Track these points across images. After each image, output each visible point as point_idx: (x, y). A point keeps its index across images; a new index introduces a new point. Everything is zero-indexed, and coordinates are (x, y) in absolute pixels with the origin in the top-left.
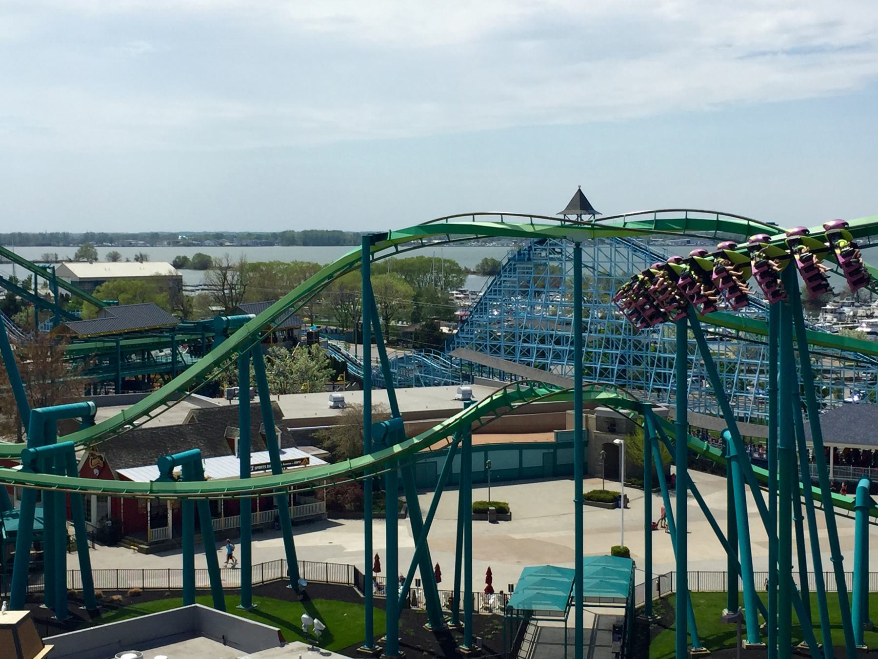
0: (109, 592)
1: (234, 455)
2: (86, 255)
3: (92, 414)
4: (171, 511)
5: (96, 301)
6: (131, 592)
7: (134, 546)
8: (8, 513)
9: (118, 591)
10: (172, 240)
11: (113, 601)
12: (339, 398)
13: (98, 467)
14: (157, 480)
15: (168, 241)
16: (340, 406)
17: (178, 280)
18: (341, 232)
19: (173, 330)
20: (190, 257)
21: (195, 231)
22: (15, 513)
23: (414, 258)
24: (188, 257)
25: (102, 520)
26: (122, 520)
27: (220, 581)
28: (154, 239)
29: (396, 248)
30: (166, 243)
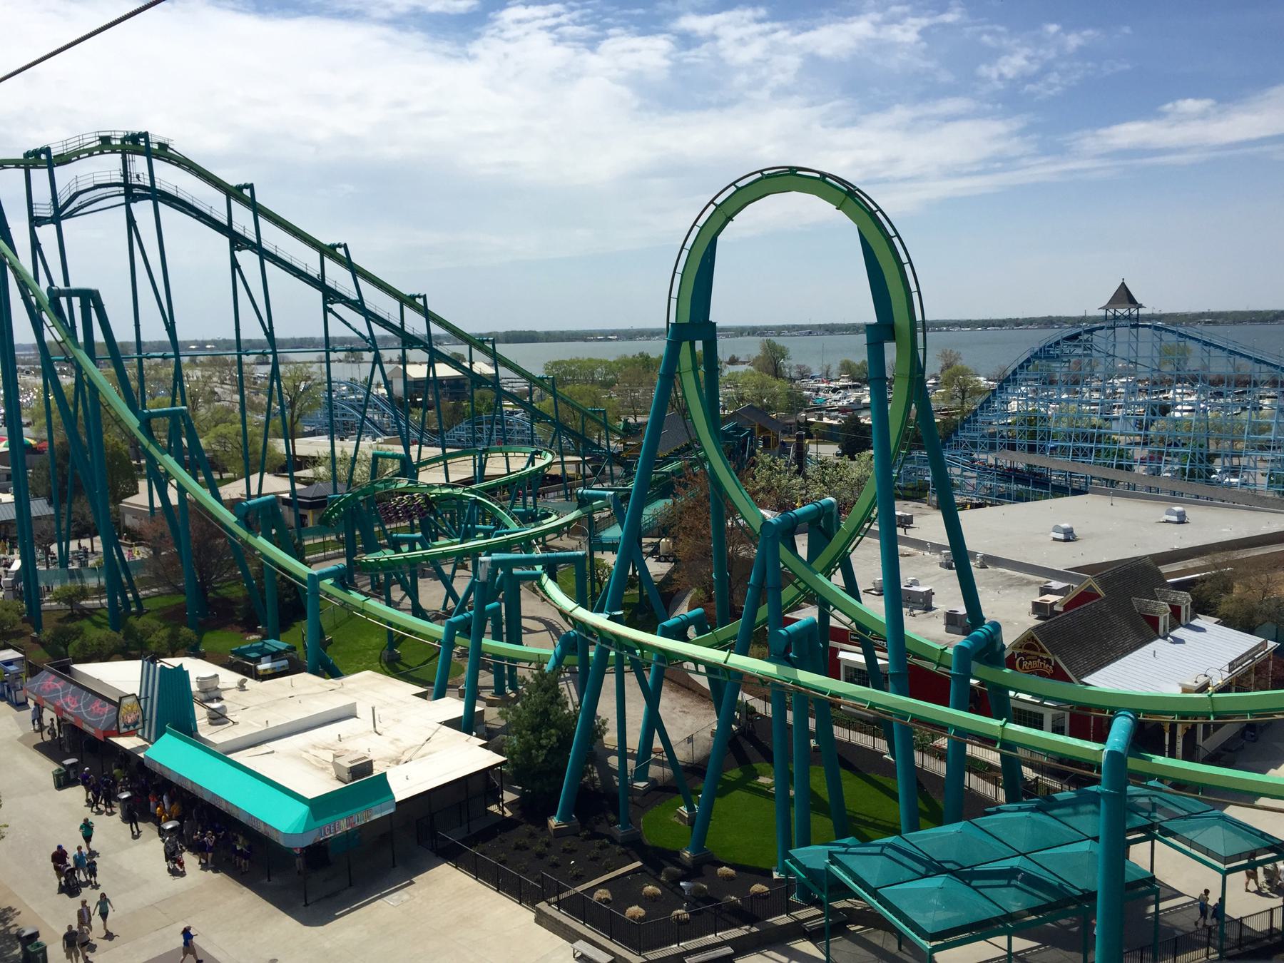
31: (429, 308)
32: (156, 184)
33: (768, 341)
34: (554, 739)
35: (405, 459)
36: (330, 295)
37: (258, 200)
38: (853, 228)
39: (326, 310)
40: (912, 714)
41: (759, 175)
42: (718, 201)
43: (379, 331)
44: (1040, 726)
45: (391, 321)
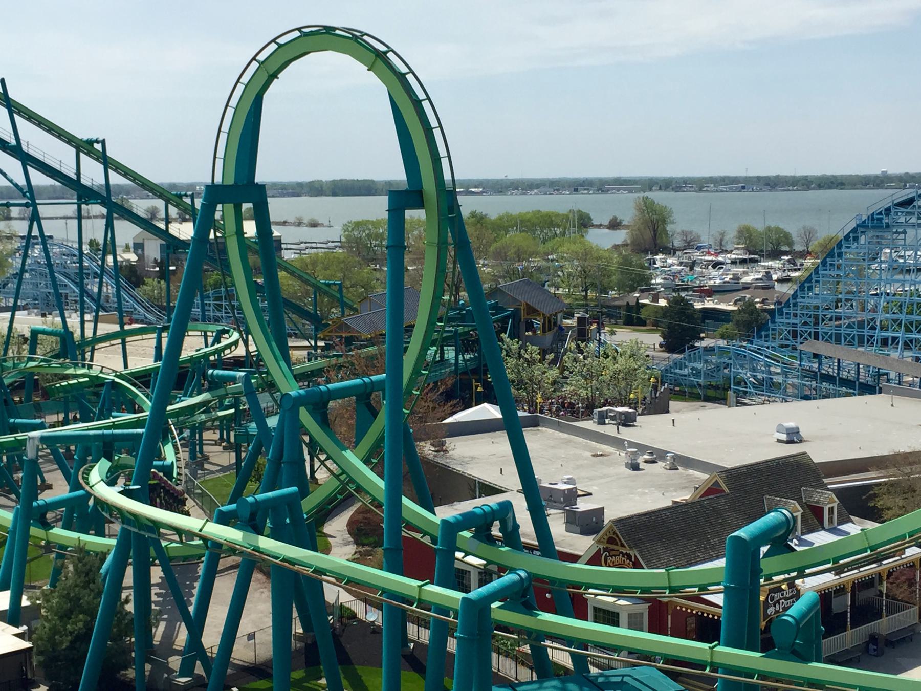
12: (793, 429)
16: (795, 440)
18: (373, 181)
21: (674, 176)
23: (529, 213)
27: (407, 634)
29: (258, 62)
33: (645, 199)
34: (80, 625)
35: (65, 336)
38: (384, 89)
40: (349, 577)
41: (297, 34)
42: (261, 57)
43: (39, 179)
44: (616, 623)
45: (64, 171)
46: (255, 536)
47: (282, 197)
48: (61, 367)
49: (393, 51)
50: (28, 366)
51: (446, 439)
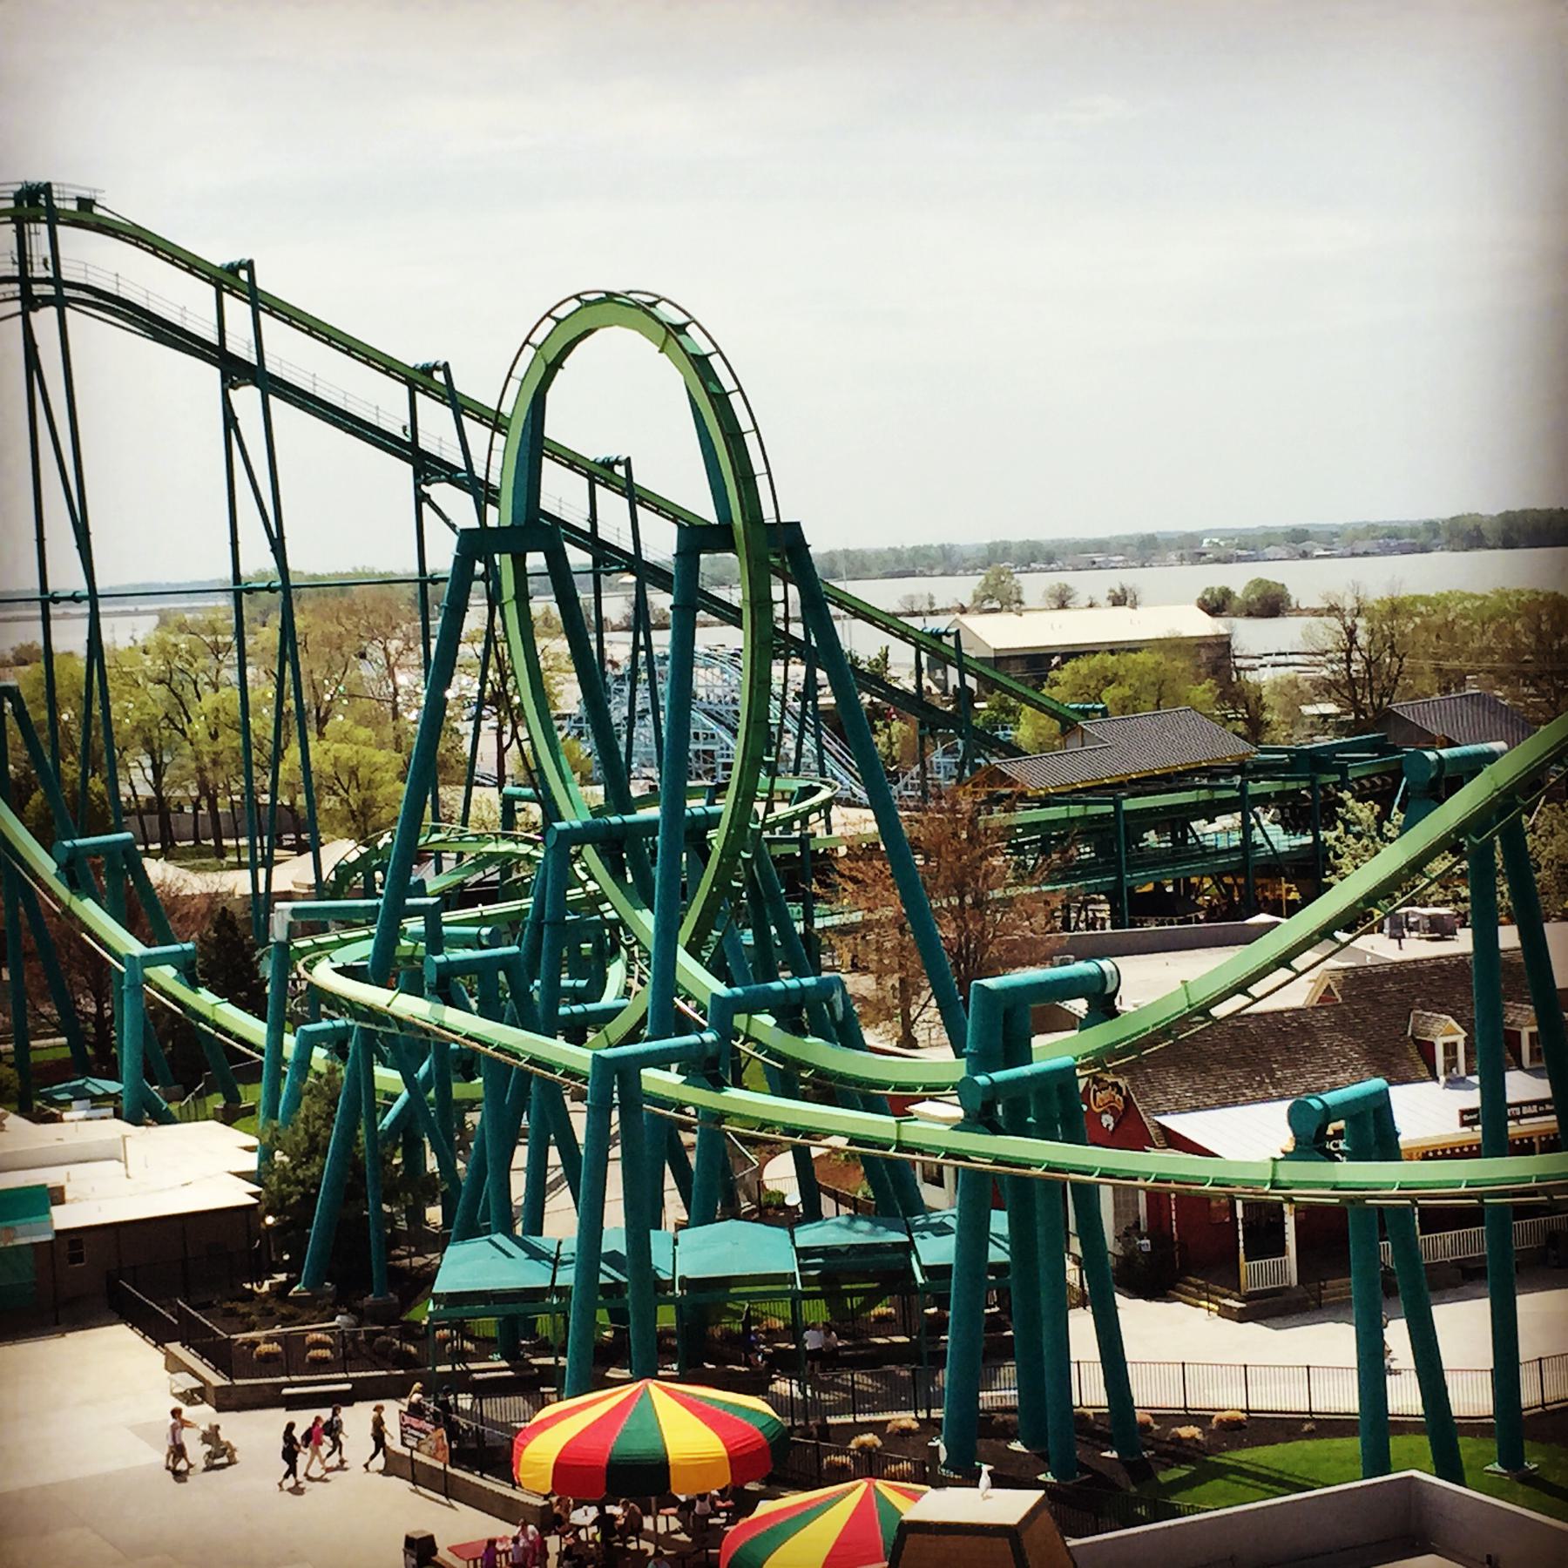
0: (1169, 1419)
1: (1436, 1079)
2: (1001, 599)
3: (1110, 989)
4: (1293, 1218)
5: (1055, 707)
6: (1220, 1421)
7: (1209, 1300)
8: (920, 1220)
9: (1188, 1416)
10: (1192, 551)
11: (1179, 1440)
13: (1113, 1111)
14: (1288, 1156)
15: (1180, 552)
17: (1222, 646)
19: (1242, 768)
20: (1239, 590)
22: (937, 1220)
24: (1232, 589)
25: (1126, 1234)
26: (1176, 1238)
28: (1147, 550)
30: (1173, 557)
31: (457, 388)
32: (643, 553)
36: (426, 467)
37: (458, 387)
39: (421, 498)
46: (442, 1006)
47: (1385, 554)
48: (478, 841)
49: (695, 322)
50: (431, 840)
51: (1125, 963)
